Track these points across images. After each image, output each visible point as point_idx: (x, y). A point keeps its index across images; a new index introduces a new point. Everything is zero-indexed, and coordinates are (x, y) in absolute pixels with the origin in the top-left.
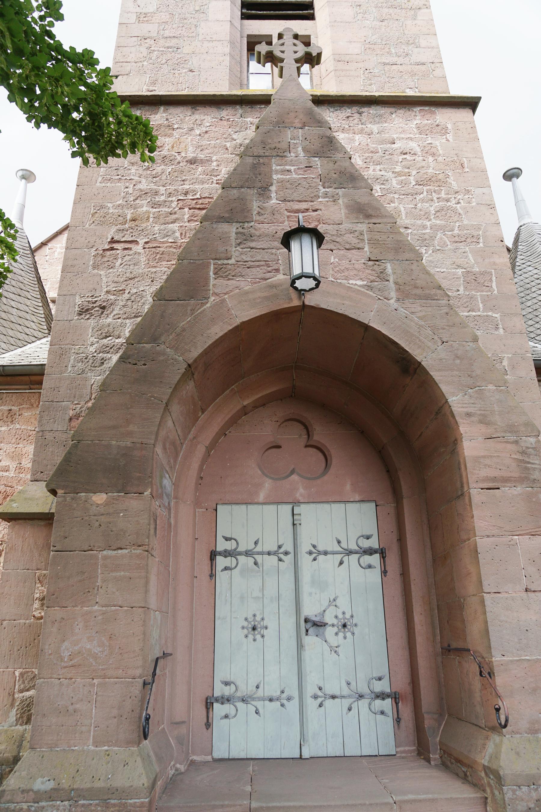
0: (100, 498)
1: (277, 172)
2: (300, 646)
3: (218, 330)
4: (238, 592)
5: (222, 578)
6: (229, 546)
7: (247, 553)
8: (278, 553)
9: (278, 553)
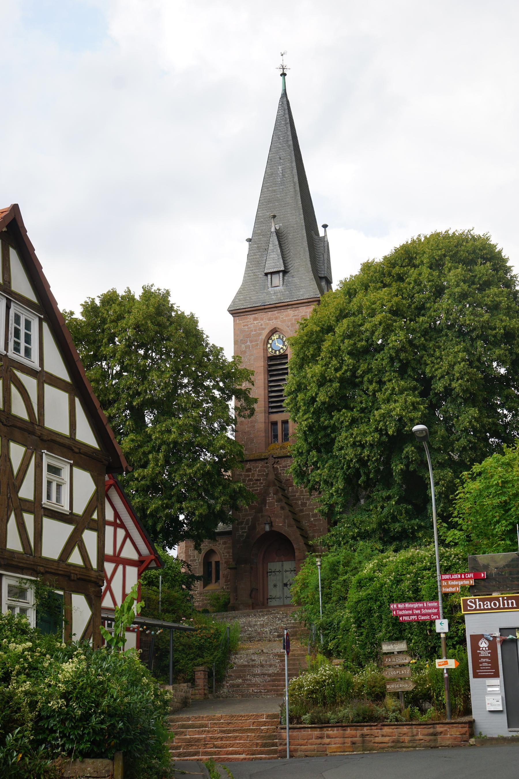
0: (243, 566)
1: (174, 755)
2: (283, 589)
3: (259, 536)
4: (272, 580)
5: (269, 577)
6: (270, 571)
7: (274, 572)
8: (279, 571)
9: (279, 571)
